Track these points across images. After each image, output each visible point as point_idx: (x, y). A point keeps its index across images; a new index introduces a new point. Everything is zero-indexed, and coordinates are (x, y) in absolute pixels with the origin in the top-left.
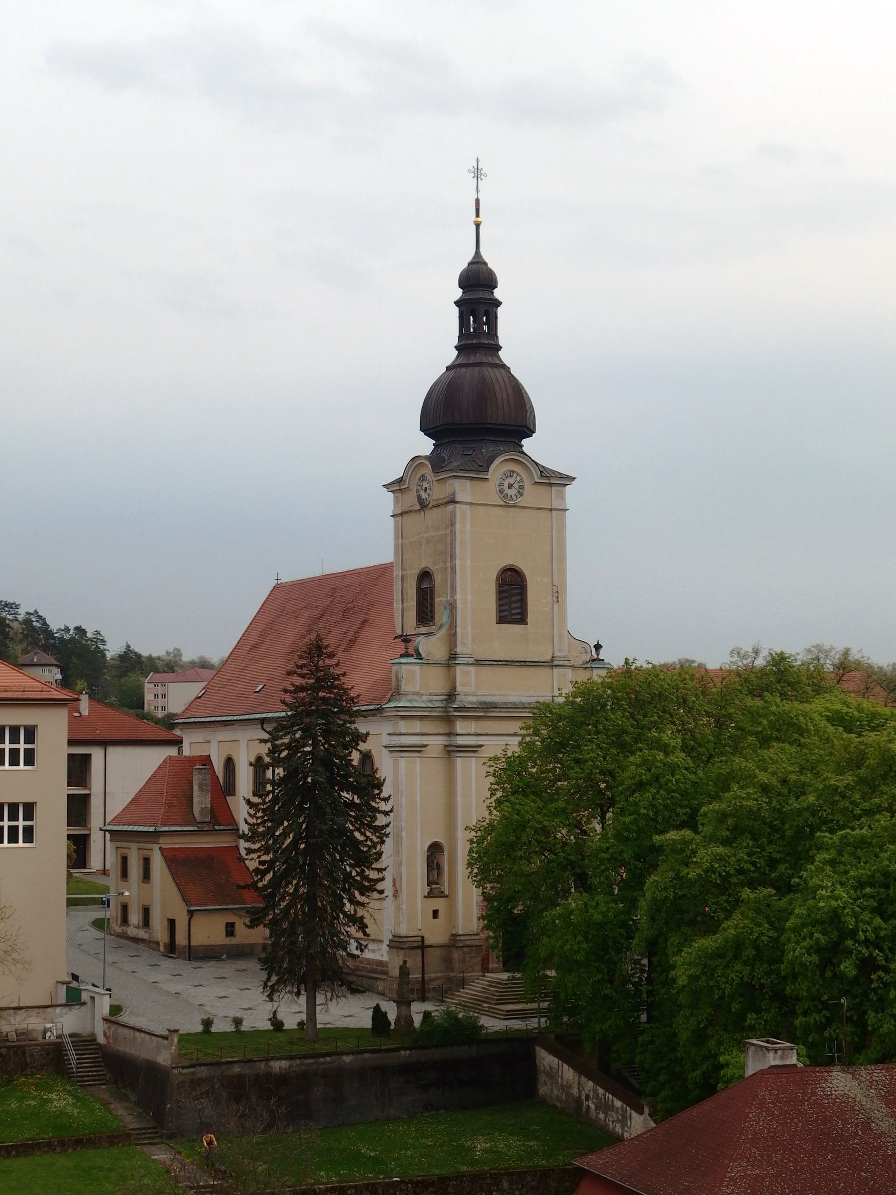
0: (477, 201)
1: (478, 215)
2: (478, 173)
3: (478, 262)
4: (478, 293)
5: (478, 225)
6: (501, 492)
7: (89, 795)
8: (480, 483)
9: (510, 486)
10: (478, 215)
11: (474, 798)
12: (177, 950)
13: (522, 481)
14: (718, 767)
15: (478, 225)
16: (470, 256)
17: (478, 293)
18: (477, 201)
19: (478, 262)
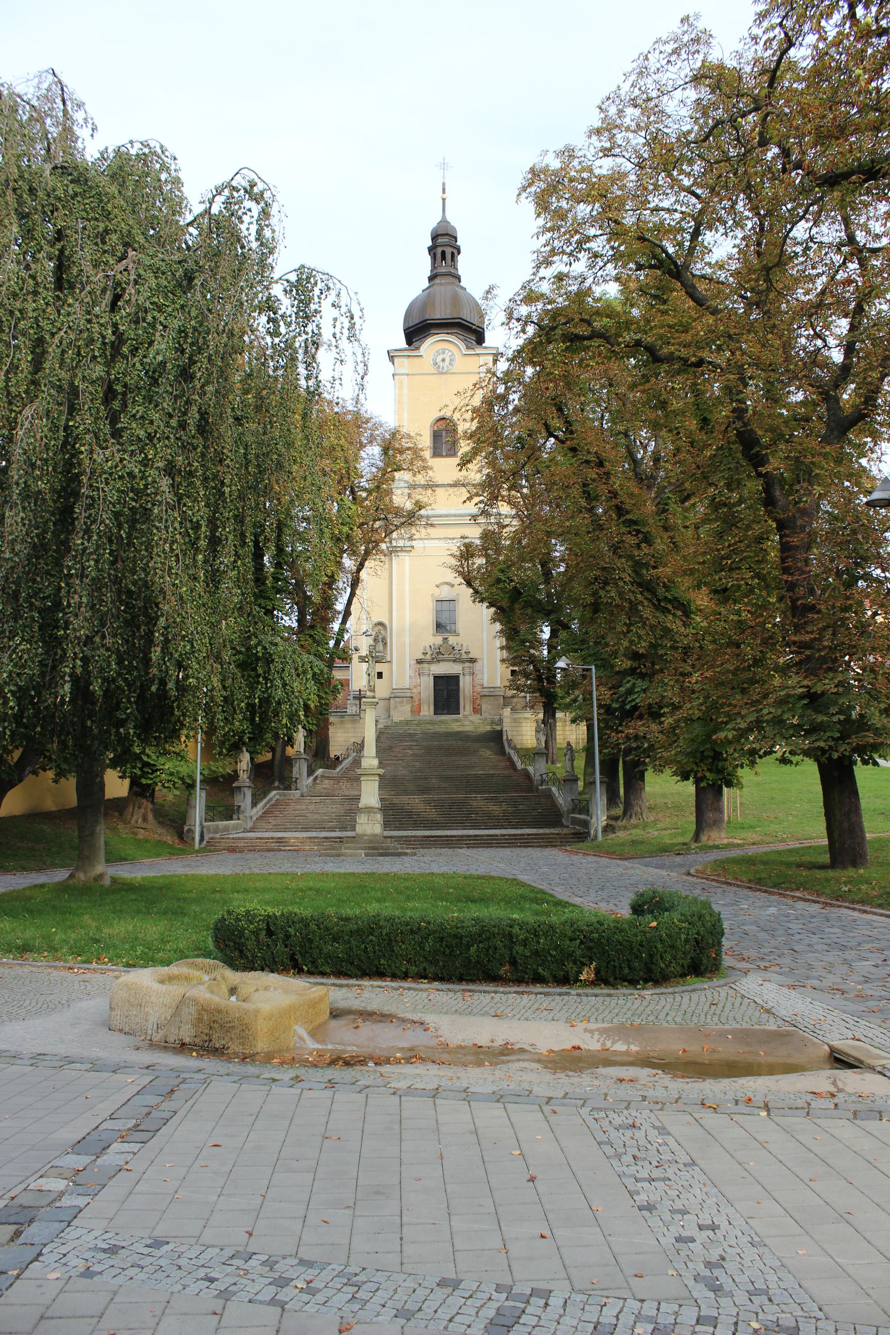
0: (444, 184)
1: (444, 192)
2: (444, 166)
3: (444, 221)
4: (444, 247)
5: (444, 200)
6: (436, 364)
7: (608, 810)
8: (416, 360)
9: (443, 360)
10: (444, 192)
11: (407, 587)
12: (870, 854)
13: (453, 355)
14: (96, 336)
15: (444, 200)
16: (439, 219)
17: (444, 247)
18: (444, 184)
19: (444, 221)
